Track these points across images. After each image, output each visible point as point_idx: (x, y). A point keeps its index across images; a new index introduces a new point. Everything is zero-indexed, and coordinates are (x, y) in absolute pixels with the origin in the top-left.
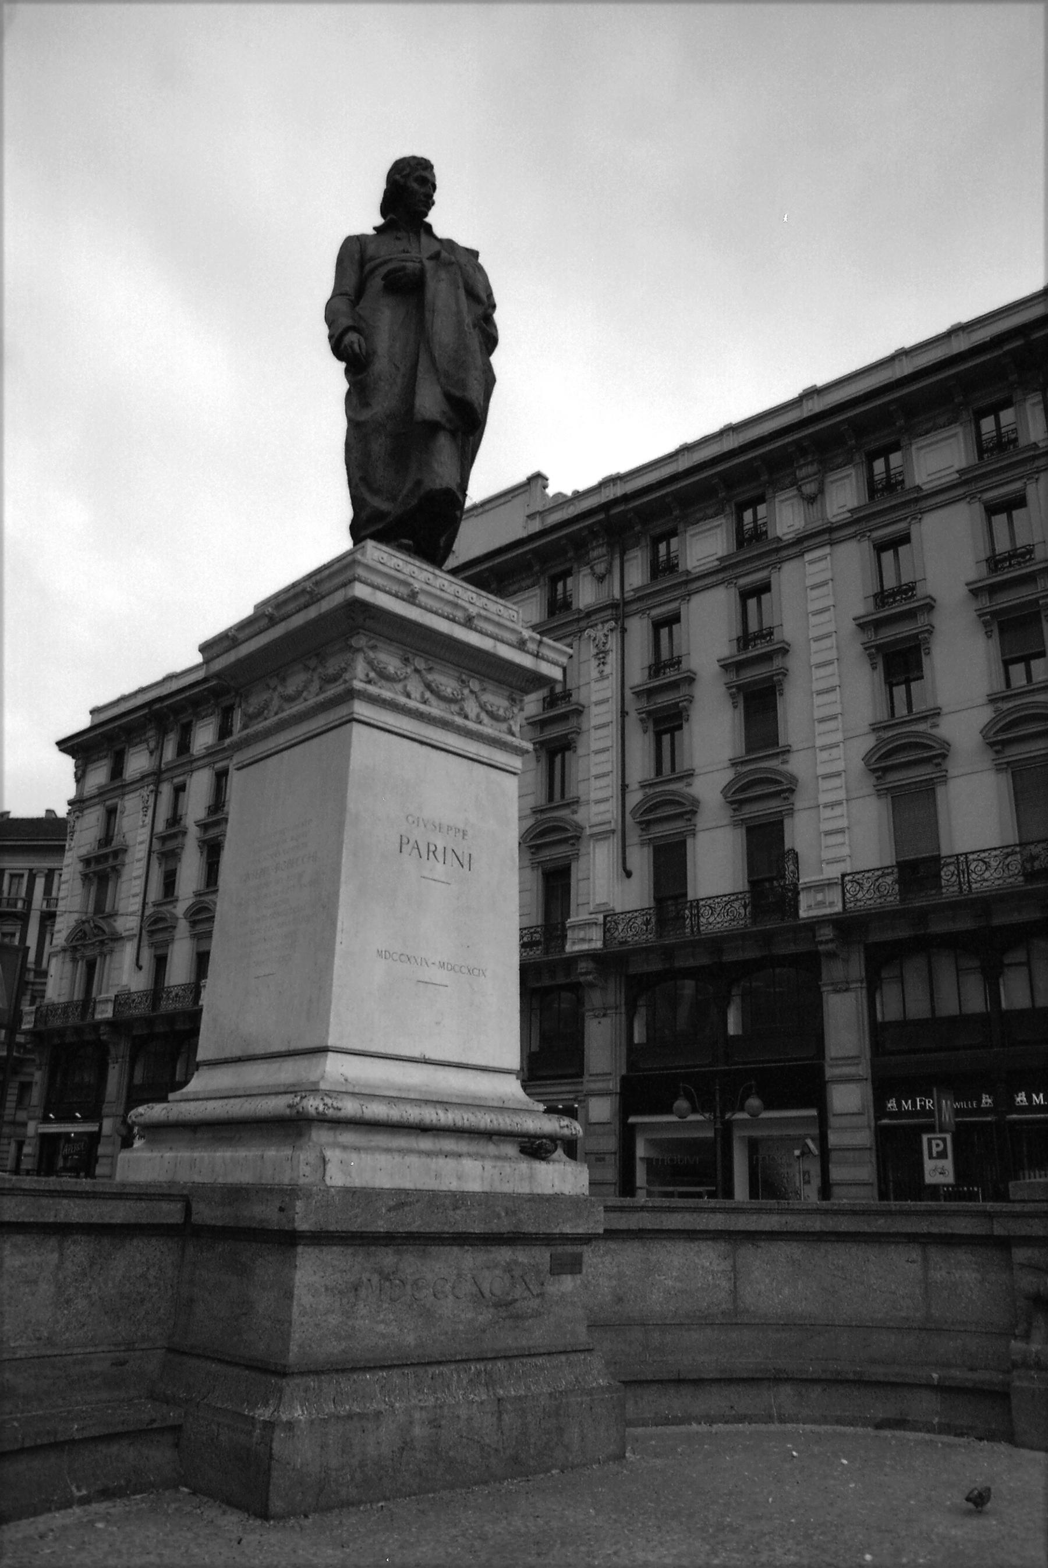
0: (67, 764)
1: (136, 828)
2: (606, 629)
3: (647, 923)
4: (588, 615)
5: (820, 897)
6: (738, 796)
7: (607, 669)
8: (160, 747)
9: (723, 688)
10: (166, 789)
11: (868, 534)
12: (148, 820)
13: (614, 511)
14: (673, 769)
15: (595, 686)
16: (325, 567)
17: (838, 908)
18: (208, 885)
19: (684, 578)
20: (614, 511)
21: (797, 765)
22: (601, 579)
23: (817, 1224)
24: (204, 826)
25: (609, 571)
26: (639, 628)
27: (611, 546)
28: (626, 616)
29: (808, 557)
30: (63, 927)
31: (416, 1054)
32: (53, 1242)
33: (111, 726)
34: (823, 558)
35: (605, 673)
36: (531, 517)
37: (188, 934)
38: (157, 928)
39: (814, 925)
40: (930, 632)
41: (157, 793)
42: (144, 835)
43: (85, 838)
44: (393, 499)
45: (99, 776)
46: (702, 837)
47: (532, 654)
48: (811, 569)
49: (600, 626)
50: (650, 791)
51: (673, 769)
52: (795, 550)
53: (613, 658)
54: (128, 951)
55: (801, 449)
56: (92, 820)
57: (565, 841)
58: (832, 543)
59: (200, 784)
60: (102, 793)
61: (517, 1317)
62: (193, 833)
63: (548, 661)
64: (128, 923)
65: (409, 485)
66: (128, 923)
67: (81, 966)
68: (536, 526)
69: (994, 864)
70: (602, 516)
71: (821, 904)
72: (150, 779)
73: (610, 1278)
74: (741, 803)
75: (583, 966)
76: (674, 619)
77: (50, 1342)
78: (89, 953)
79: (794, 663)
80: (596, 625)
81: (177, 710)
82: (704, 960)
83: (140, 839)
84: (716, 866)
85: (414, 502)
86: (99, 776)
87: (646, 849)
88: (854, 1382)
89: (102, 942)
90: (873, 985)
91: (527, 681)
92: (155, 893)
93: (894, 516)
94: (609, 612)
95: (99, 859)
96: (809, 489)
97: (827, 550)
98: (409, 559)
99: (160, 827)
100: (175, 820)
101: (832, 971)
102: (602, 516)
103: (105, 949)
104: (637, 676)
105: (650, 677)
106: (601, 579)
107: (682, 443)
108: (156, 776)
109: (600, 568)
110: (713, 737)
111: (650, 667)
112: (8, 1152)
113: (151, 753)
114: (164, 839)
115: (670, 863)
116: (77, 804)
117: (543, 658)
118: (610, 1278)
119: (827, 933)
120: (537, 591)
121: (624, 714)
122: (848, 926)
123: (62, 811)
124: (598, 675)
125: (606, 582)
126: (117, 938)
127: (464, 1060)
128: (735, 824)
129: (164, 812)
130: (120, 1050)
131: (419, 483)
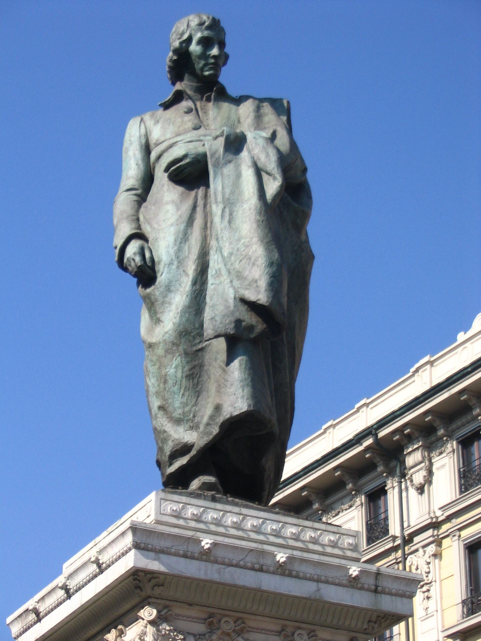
2: (427, 555)
11: (458, 533)
13: (382, 433)
19: (391, 545)
20: (382, 433)
35: (429, 611)
44: (194, 427)
47: (368, 590)
49: (421, 551)
63: (391, 594)
65: (209, 411)
70: (369, 441)
80: (417, 550)
85: (215, 430)
91: (370, 621)
94: (430, 532)
102: (369, 441)
107: (472, 328)
111: (464, 602)
117: (383, 592)
124: (424, 613)
131: (218, 408)
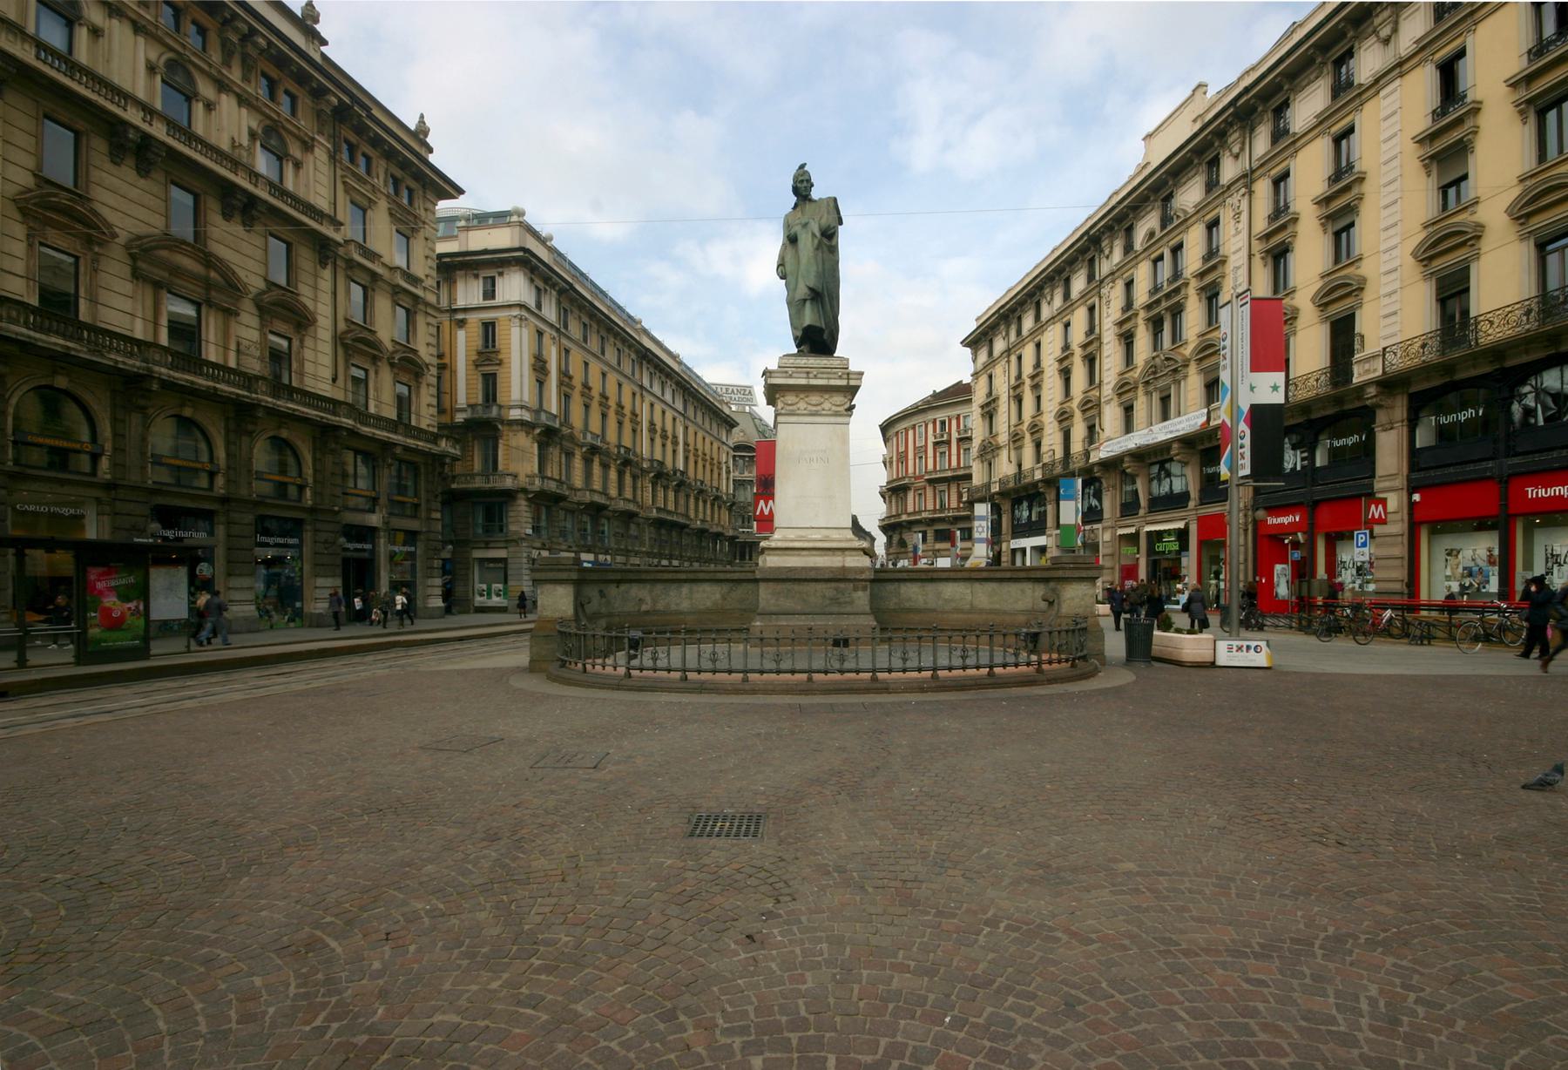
0: (968, 350)
1: (1002, 387)
3: (1528, 313)
4: (1229, 187)
5: (1367, 366)
6: (1325, 300)
7: (1240, 226)
8: (1007, 334)
9: (1511, 107)
10: (1013, 358)
14: (1561, 151)
15: (1233, 240)
17: (1380, 372)
18: (1210, 324)
21: (1365, 269)
22: (1237, 157)
23: (1008, 575)
24: (1033, 377)
25: (1242, 149)
26: (1263, 188)
27: (1243, 128)
28: (1252, 182)
29: (1382, 93)
30: (976, 443)
34: (1395, 90)
36: (1195, 121)
37: (1316, 320)
38: (1016, 439)
39: (1362, 388)
40: (1476, 133)
43: (979, 396)
45: (983, 357)
46: (1299, 334)
48: (1384, 103)
50: (1431, 229)
51: (1561, 151)
52: (1372, 91)
53: (1244, 217)
54: (1004, 454)
55: (1229, 124)
56: (984, 380)
57: (1463, 244)
58: (1401, 75)
59: (1028, 352)
60: (986, 366)
62: (1078, 352)
64: (1003, 438)
66: (1003, 438)
68: (1198, 126)
69: (1496, 321)
71: (1368, 371)
74: (1326, 305)
75: (1175, 446)
76: (1286, 175)
78: (1160, 384)
79: (1368, 188)
81: (1013, 310)
82: (1487, 369)
84: (1310, 350)
86: (983, 357)
87: (1525, 244)
89: (1175, 371)
90: (1412, 424)
92: (1014, 421)
93: (1278, 160)
95: (988, 404)
96: (1385, 32)
97: (1397, 82)
98: (1198, 107)
99: (1013, 381)
100: (1019, 377)
101: (1381, 417)
103: (1178, 377)
104: (1261, 225)
105: (1530, 61)
106: (1237, 157)
109: (1236, 149)
110: (1310, 258)
114: (1015, 388)
115: (1452, 292)
116: (976, 375)
119: (1372, 391)
120: (1197, 178)
121: (1250, 256)
122: (1389, 384)
123: (967, 379)
125: (1392, 44)
126: (999, 448)
128: (1522, 238)
129: (1014, 373)
130: (1399, 409)
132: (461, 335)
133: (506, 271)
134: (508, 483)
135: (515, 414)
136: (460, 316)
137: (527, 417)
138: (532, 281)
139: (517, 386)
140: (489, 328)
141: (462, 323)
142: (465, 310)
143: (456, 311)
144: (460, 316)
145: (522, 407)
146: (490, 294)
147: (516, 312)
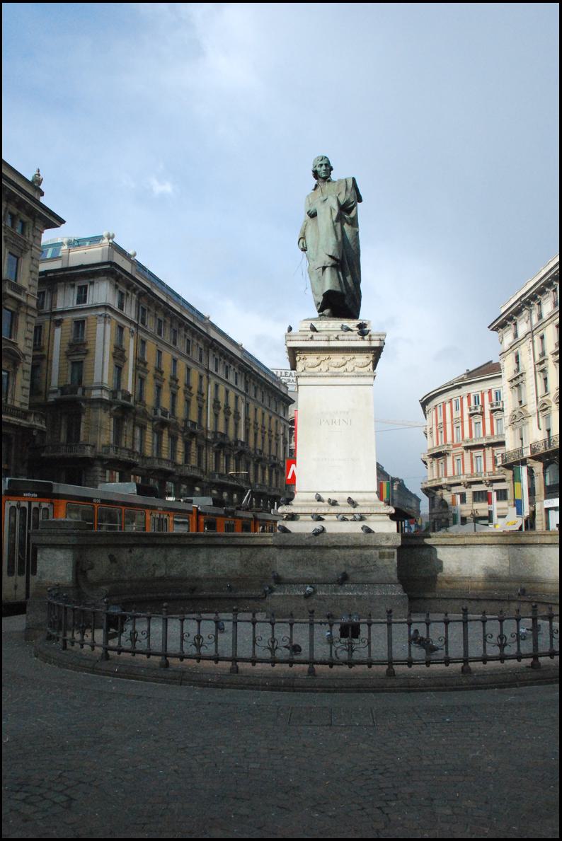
10: (537, 338)
12: (532, 356)
16: (261, 364)
31: (330, 490)
32: (239, 549)
33: (500, 320)
41: (533, 342)
42: (531, 364)
61: (365, 572)
64: (532, 407)
66: (532, 407)
67: (517, 431)
72: (530, 334)
73: (456, 562)
77: (240, 575)
83: (530, 366)
88: (496, 600)
92: (541, 392)
108: (531, 333)
112: (256, 531)
113: (527, 322)
118: (456, 562)
127: (351, 490)
129: (538, 351)
132: (58, 331)
133: (95, 281)
134: (88, 452)
135: (96, 394)
136: (58, 317)
137: (106, 396)
138: (116, 287)
139: (101, 370)
140: (80, 324)
141: (59, 323)
142: (63, 312)
143: (55, 313)
144: (58, 317)
145: (102, 388)
146: (82, 298)
147: (101, 312)
